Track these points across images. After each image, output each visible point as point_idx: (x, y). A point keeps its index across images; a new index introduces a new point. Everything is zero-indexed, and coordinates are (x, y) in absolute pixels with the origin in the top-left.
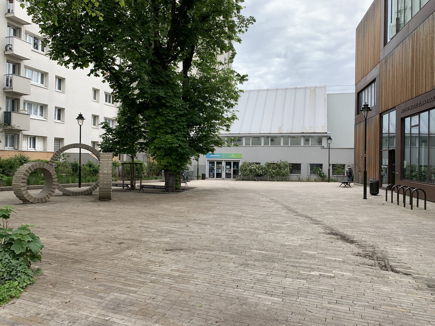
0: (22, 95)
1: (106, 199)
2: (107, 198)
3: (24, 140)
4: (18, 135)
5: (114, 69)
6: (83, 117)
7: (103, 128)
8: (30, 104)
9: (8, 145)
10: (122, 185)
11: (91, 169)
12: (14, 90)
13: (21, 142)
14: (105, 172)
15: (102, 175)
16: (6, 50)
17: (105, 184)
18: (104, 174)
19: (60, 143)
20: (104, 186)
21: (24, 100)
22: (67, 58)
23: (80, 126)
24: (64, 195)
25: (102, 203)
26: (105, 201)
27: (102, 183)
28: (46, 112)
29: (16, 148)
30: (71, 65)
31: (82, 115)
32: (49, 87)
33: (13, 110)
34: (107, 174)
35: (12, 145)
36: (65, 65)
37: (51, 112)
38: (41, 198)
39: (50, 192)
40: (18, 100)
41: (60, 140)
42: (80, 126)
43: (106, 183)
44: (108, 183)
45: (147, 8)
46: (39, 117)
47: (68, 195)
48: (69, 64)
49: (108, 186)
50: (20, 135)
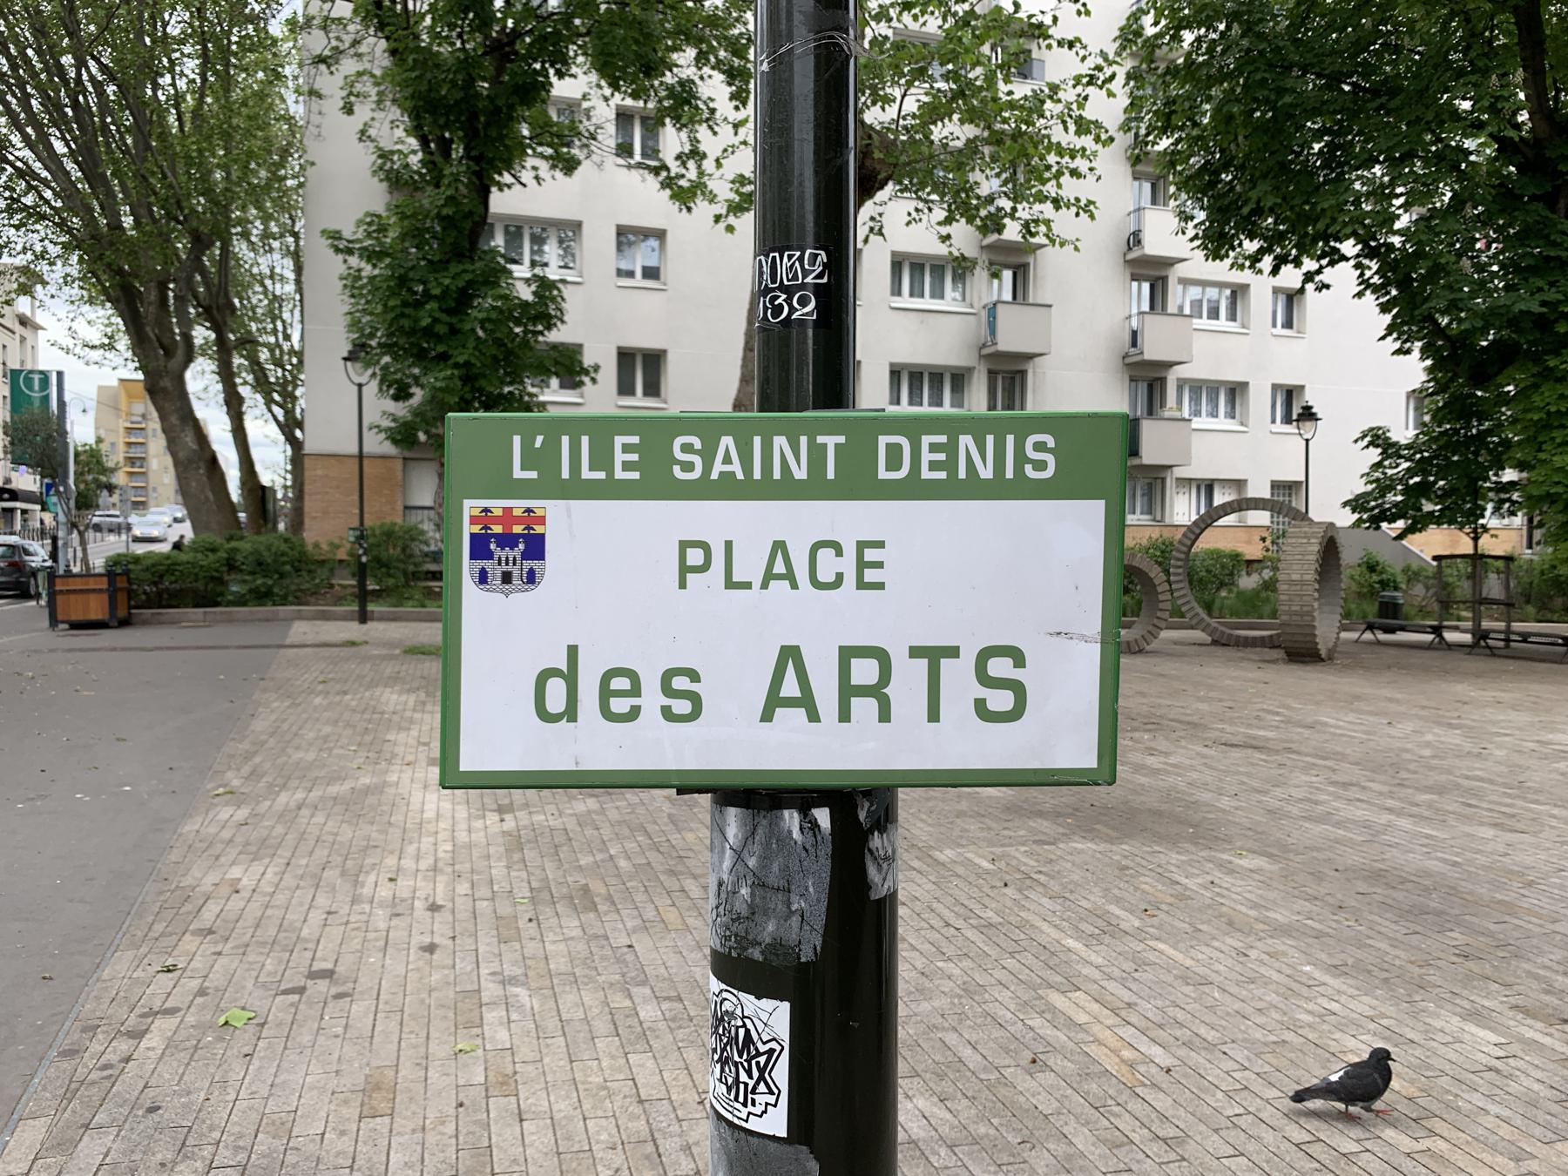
0: (1170, 365)
1: (1308, 659)
2: (1311, 656)
3: (1180, 495)
4: (1163, 480)
5: (1390, 247)
6: (1314, 414)
7: (1371, 444)
8: (1197, 388)
9: (1138, 510)
10: (1502, 636)
11: (1375, 578)
12: (1147, 356)
13: (1171, 498)
14: (1294, 577)
15: (1286, 587)
16: (1130, 249)
17: (1296, 613)
18: (1291, 582)
19: (1290, 495)
20: (1294, 618)
21: (1178, 379)
22: (1251, 246)
23: (1307, 441)
24: (1215, 643)
25: (1294, 667)
26: (1303, 662)
27: (1287, 608)
28: (1245, 403)
29: (1159, 518)
30: (1267, 262)
31: (1311, 407)
32: (1252, 327)
33: (1150, 412)
34: (1302, 583)
35: (1149, 510)
36: (1252, 266)
37: (1260, 400)
38: (1128, 643)
39: (1150, 628)
40: (1163, 381)
41: (1290, 488)
42: (1307, 441)
43: (1298, 608)
44: (1305, 609)
45: (1456, 31)
46: (1222, 423)
47: (1224, 645)
48: (1260, 260)
49: (1306, 618)
50: (1168, 481)
